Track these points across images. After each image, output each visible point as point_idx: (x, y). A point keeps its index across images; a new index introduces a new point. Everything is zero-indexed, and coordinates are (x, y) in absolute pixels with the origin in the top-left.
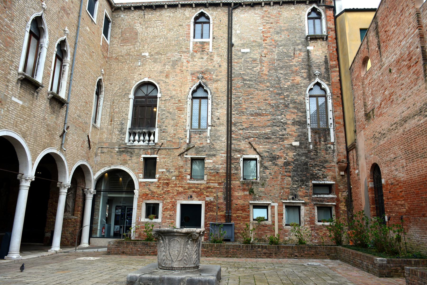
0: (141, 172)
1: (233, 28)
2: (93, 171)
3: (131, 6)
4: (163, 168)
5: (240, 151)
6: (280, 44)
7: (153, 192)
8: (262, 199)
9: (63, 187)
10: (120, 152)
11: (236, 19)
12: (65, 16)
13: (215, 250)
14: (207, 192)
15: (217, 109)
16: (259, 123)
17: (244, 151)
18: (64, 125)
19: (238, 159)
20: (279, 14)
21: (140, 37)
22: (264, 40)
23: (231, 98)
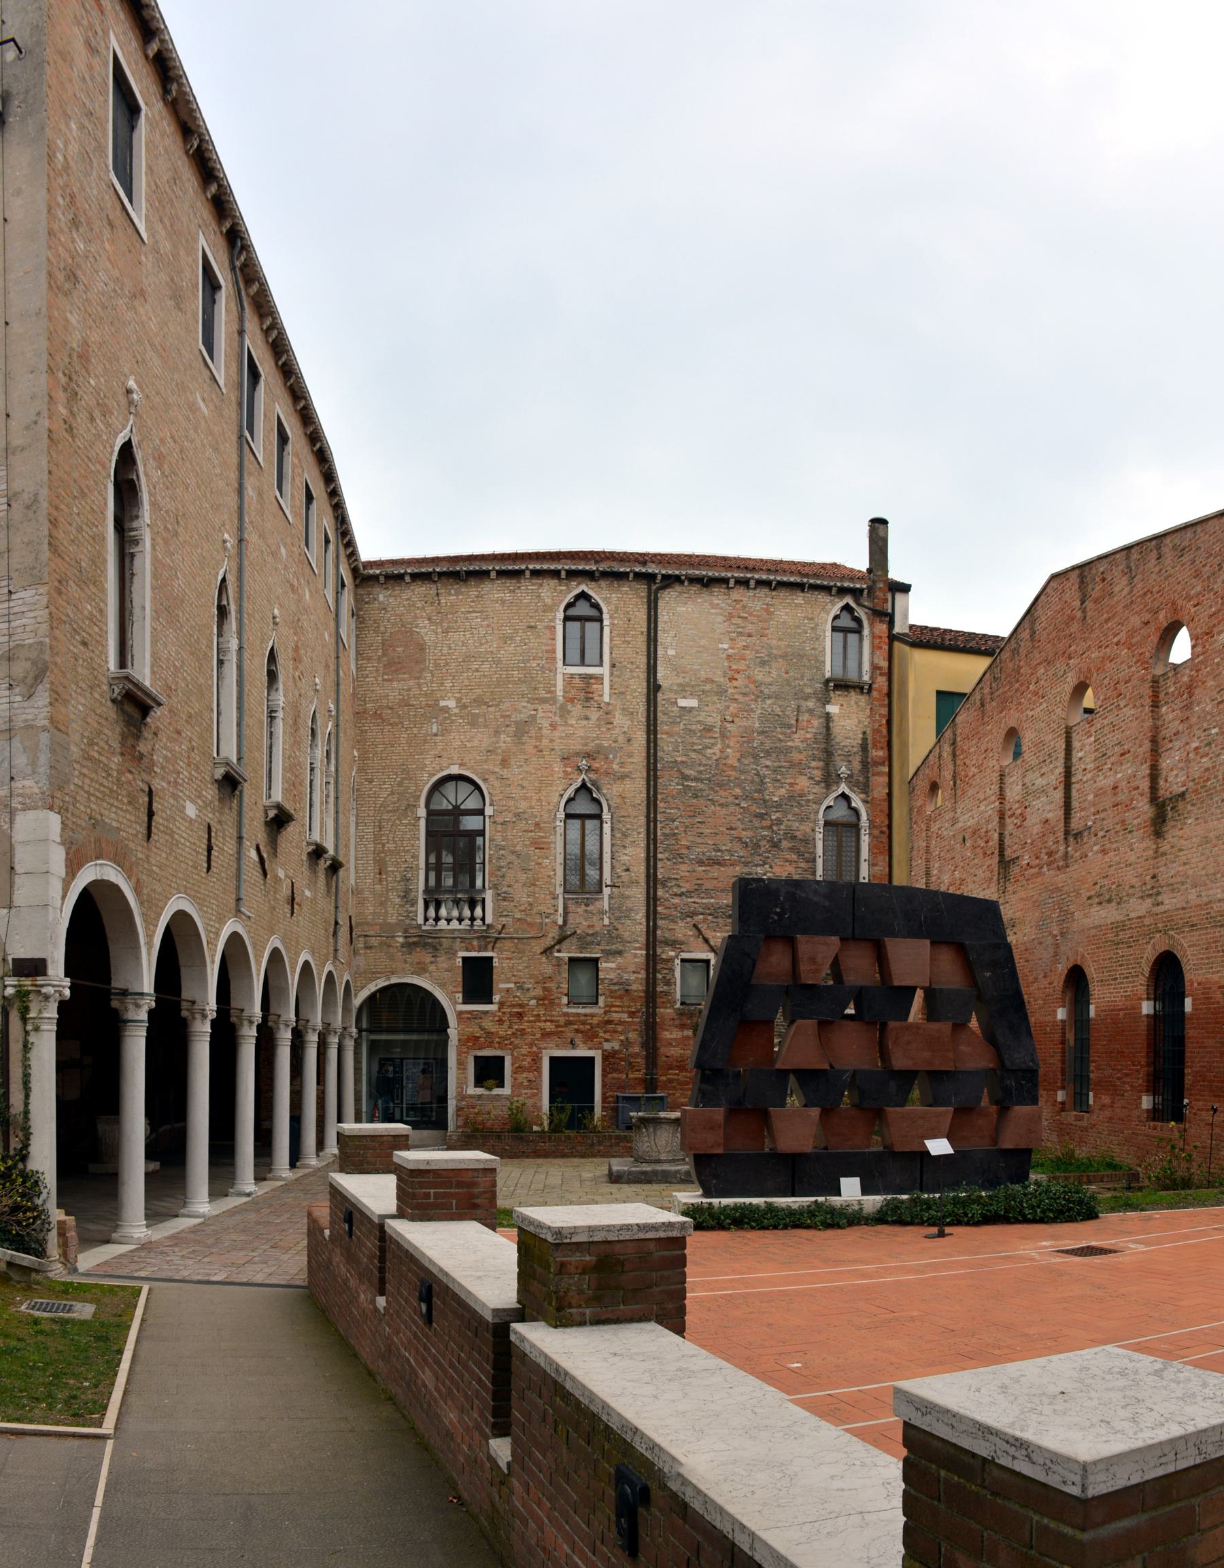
4: (508, 981)
5: (673, 944)
10: (409, 946)
17: (682, 943)
19: (671, 960)
20: (767, 611)
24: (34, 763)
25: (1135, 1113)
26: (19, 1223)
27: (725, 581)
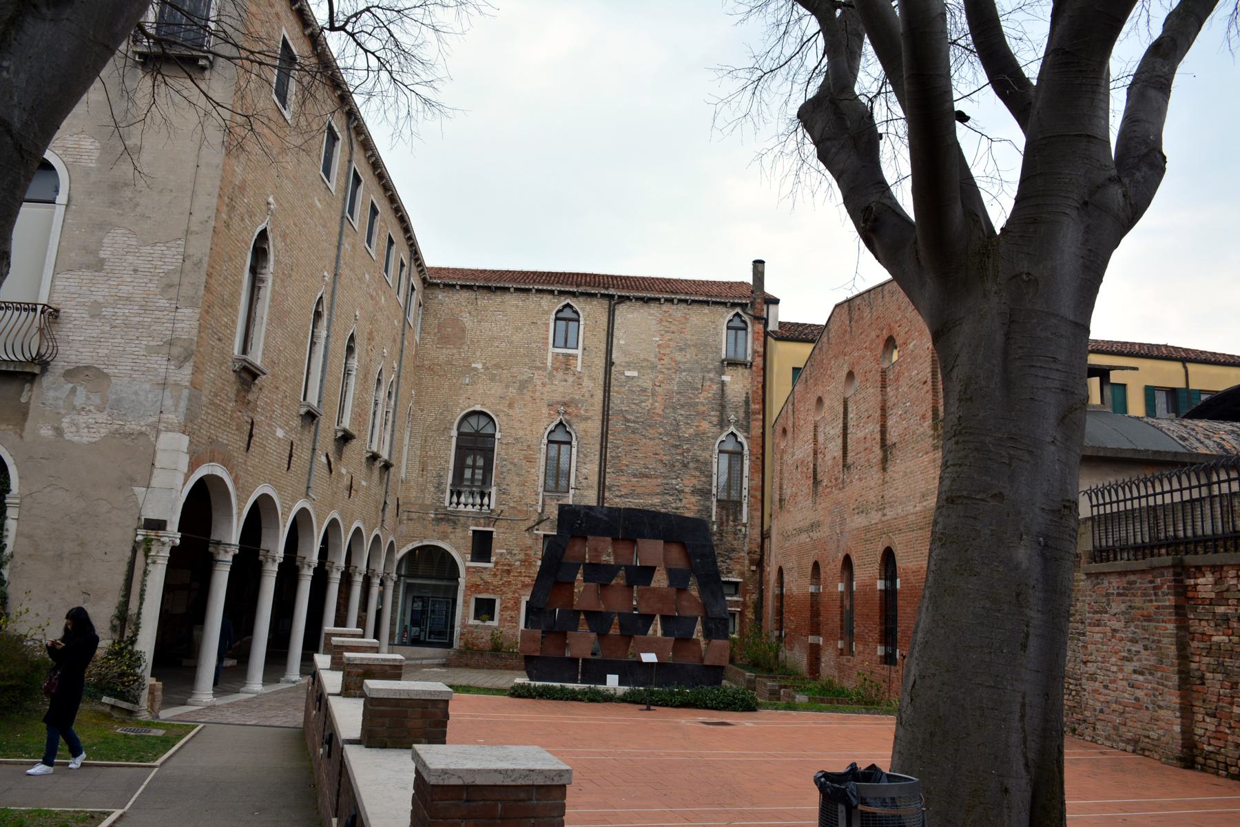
10: (438, 520)
24: (176, 406)
25: (874, 658)
26: (123, 683)
27: (658, 300)
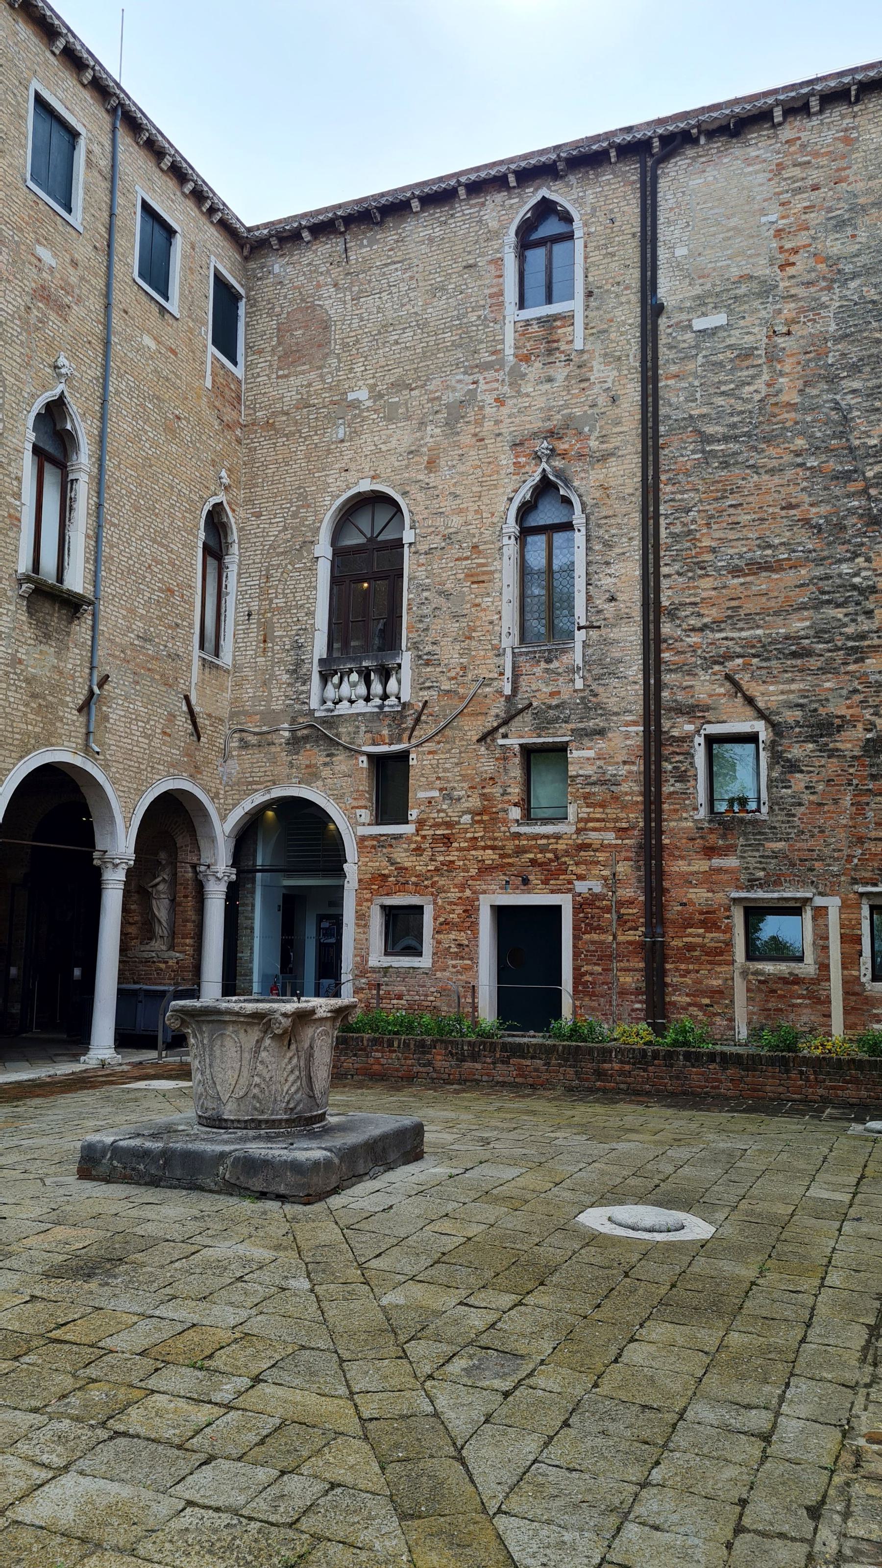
0: (363, 803)
1: (661, 237)
2: (218, 809)
3: (300, 228)
4: (430, 786)
5: (692, 711)
6: (849, 268)
7: (402, 869)
8: (777, 883)
9: (110, 865)
10: (295, 743)
11: (671, 203)
12: (53, 316)
13: (560, 1065)
14: (577, 864)
15: (607, 563)
16: (764, 599)
17: (707, 708)
18: (91, 674)
19: (687, 739)
20: (847, 141)
21: (336, 335)
22: (782, 267)
23: (657, 515)
